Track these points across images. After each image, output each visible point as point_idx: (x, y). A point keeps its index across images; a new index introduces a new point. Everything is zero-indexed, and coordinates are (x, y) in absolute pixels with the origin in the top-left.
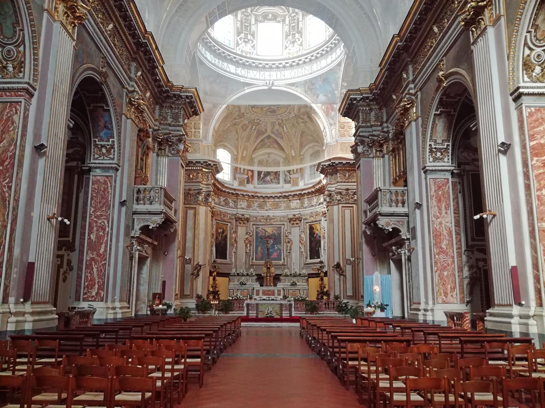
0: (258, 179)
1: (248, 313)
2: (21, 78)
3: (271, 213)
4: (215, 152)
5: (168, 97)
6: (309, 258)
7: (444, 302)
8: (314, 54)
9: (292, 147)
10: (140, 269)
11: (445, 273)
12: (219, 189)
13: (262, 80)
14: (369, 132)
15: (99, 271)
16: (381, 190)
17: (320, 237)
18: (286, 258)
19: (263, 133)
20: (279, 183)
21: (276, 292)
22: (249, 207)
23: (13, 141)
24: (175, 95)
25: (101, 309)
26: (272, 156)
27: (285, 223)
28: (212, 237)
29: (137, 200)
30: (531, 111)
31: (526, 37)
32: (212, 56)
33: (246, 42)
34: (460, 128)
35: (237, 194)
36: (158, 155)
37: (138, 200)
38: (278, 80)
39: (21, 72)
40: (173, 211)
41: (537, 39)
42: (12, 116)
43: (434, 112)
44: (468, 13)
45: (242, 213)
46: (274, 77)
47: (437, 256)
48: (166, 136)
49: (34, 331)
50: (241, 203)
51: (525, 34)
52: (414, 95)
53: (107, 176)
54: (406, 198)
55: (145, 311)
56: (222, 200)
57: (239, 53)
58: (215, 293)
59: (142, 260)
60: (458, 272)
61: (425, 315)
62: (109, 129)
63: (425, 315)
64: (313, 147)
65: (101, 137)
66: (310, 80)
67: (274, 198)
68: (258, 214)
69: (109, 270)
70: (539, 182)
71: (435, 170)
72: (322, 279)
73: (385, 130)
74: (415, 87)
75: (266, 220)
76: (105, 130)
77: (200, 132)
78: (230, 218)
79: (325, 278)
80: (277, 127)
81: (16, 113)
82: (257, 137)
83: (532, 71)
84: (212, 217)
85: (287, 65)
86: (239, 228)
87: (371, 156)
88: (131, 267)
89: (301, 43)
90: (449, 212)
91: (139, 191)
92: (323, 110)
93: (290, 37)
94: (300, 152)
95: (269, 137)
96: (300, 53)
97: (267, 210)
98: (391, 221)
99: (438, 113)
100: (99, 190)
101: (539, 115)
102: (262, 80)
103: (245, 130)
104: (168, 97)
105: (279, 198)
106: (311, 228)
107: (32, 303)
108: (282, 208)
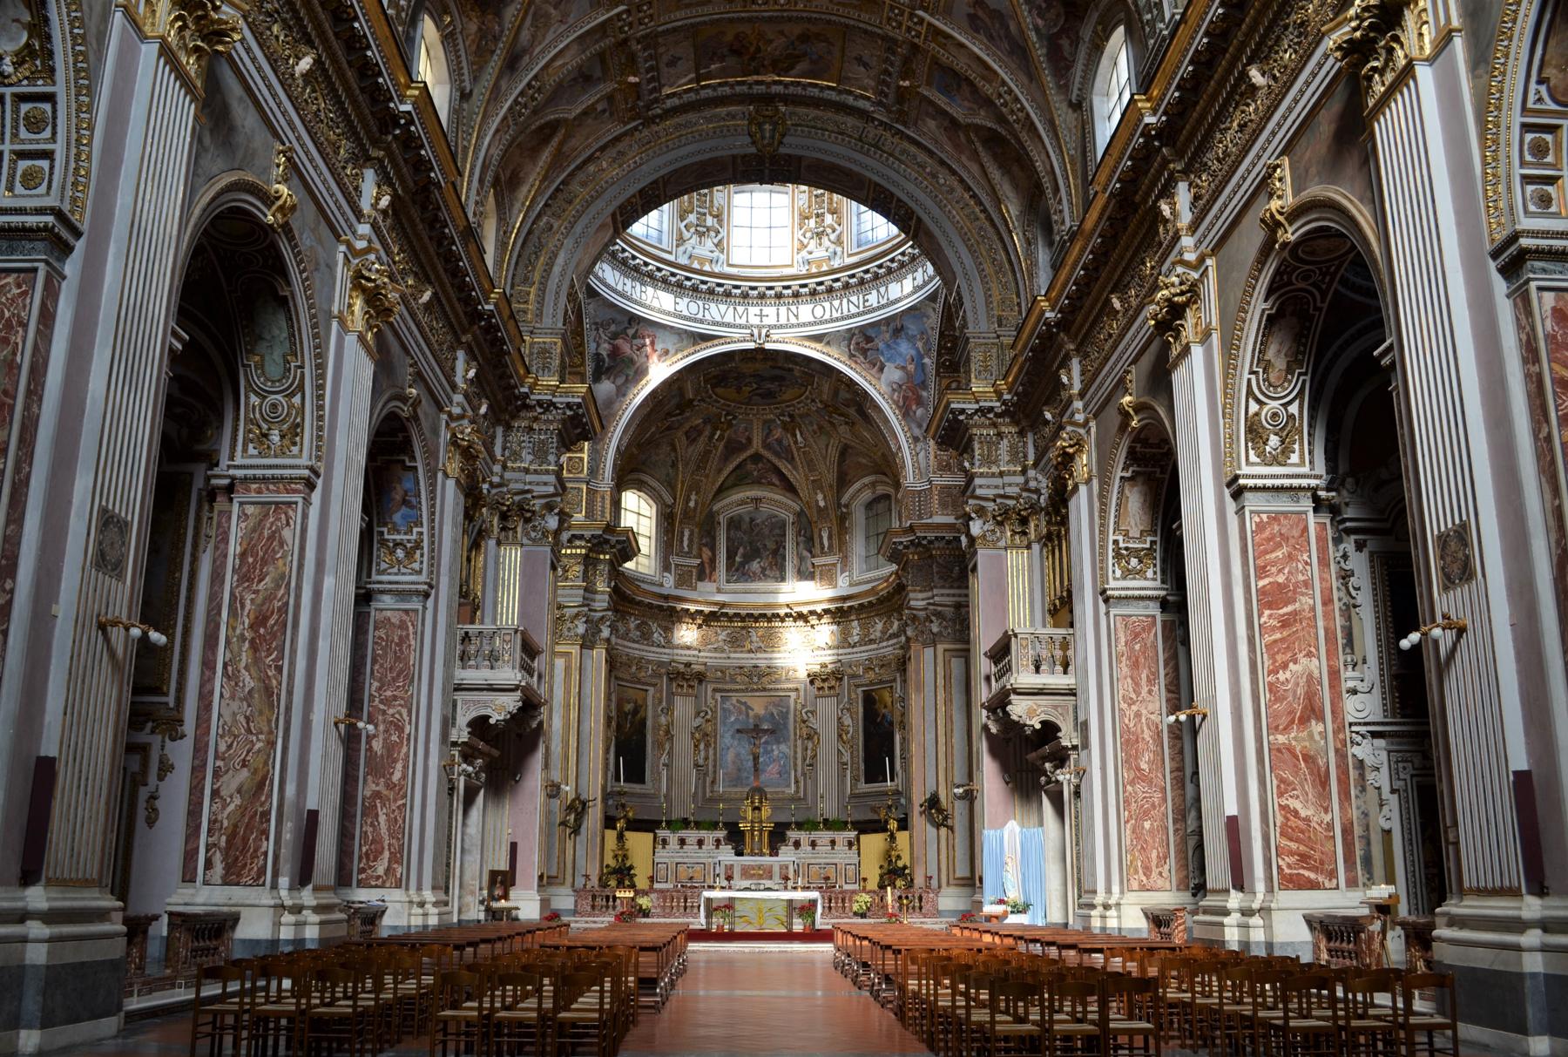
2: (294, 457)
4: (617, 504)
7: (1143, 888)
9: (817, 485)
11: (1147, 825)
13: (740, 327)
17: (891, 724)
21: (776, 870)
23: (282, 579)
24: (540, 403)
25: (398, 906)
29: (462, 659)
31: (1249, 380)
32: (617, 274)
33: (701, 235)
34: (1336, 356)
36: (499, 543)
37: (464, 657)
38: (781, 327)
39: (295, 444)
41: (1270, 385)
42: (278, 530)
43: (1119, 474)
44: (1353, 24)
45: (685, 659)
46: (771, 320)
48: (517, 498)
49: (321, 940)
51: (1246, 376)
52: (1195, 268)
53: (406, 611)
55: (476, 913)
56: (632, 626)
57: (683, 261)
58: (623, 874)
61: (1103, 917)
62: (412, 507)
63: (1103, 917)
64: (873, 484)
70: (1272, 657)
71: (1127, 598)
72: (893, 837)
73: (1033, 484)
74: (1085, 408)
75: (750, 676)
76: (404, 510)
77: (581, 459)
80: (778, 433)
81: (288, 524)
82: (726, 458)
83: (1265, 444)
85: (803, 290)
86: (678, 700)
87: (1002, 544)
88: (451, 813)
89: (839, 237)
91: (466, 638)
92: (896, 403)
94: (839, 499)
95: (757, 458)
96: (836, 263)
97: (750, 651)
99: (1128, 474)
100: (389, 641)
101: (1276, 528)
102: (740, 327)
103: (694, 440)
106: (869, 700)
107: (315, 889)
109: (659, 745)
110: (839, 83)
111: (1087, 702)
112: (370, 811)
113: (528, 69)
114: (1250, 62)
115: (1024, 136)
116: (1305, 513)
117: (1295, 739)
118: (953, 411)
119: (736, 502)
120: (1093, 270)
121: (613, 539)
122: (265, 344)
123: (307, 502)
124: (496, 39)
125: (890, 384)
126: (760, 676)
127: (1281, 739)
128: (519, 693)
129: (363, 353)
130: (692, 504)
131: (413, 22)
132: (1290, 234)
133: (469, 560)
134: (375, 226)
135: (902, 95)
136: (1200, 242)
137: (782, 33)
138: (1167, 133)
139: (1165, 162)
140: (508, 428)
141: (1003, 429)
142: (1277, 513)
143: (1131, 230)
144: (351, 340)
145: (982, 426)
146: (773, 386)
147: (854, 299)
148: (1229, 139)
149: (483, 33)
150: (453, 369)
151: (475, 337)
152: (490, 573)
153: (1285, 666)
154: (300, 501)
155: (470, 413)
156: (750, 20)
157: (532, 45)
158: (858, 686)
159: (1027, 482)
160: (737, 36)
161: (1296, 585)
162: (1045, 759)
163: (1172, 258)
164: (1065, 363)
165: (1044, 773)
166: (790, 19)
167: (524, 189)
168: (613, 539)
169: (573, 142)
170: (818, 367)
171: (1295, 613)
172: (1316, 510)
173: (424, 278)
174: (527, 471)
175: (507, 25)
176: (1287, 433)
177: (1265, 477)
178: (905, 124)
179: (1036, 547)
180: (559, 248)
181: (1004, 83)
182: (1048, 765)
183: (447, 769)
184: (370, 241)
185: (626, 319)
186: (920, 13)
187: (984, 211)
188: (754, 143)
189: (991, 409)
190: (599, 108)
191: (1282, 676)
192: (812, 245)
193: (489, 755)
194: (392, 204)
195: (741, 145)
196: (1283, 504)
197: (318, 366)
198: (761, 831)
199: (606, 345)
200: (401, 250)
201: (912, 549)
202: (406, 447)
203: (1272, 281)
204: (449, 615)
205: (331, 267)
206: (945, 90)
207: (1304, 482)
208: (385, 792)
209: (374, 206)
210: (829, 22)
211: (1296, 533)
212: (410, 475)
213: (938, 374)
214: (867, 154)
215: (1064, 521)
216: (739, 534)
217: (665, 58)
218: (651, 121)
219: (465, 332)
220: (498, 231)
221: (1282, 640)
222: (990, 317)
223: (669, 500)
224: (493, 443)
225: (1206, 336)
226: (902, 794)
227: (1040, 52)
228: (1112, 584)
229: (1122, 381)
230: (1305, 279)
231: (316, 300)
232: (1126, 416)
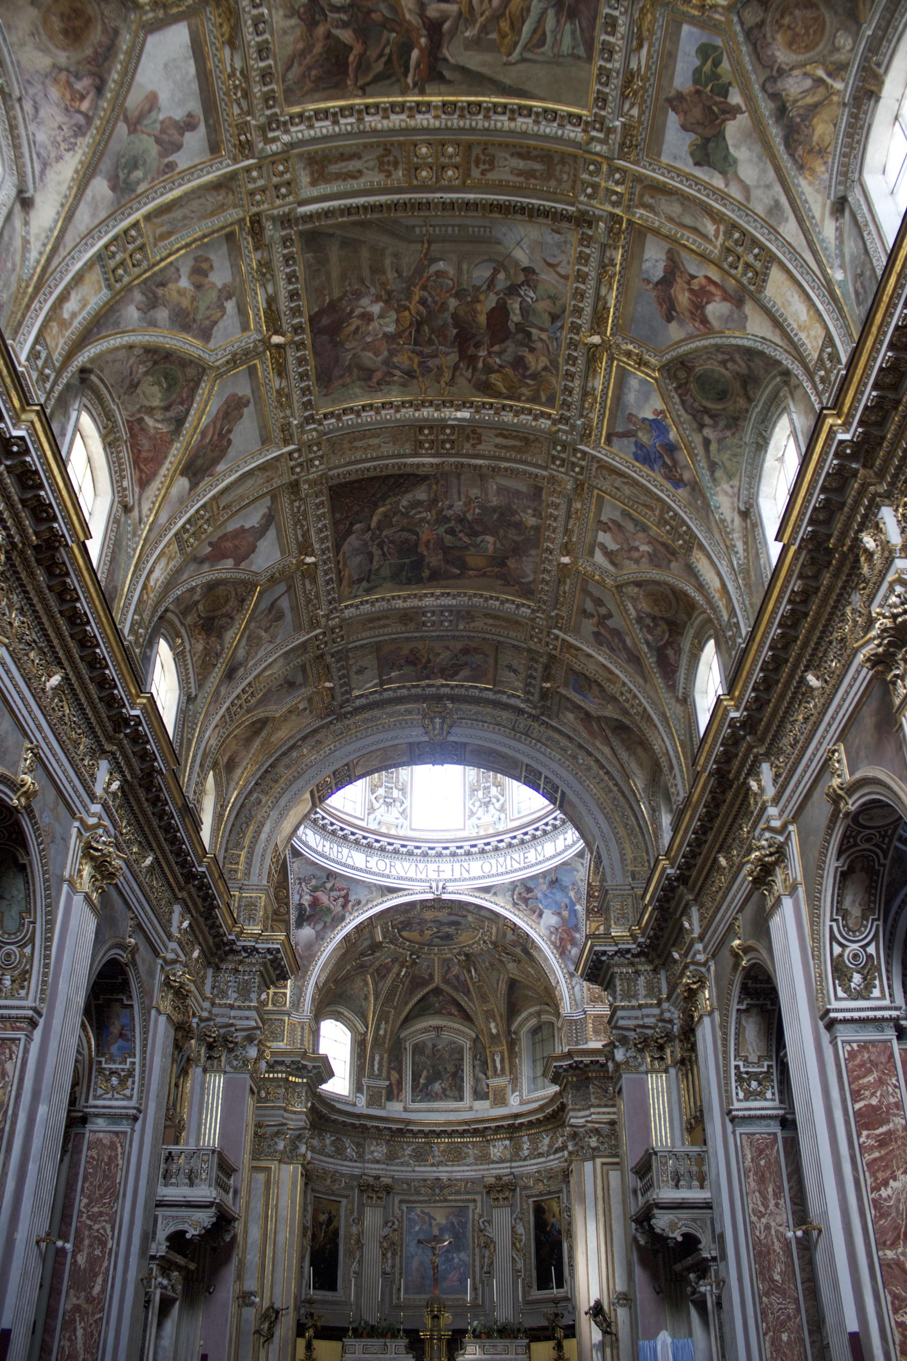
0: (414, 1089)
2: (21, 999)
3: (444, 1173)
4: (316, 1033)
5: (232, 951)
6: (535, 1286)
8: (530, 830)
10: (160, 1325)
12: (325, 1116)
15: (88, 1335)
16: (656, 1153)
17: (559, 1232)
18: (480, 1286)
19: (424, 983)
22: (391, 1157)
24: (244, 949)
26: (445, 1035)
27: (478, 1197)
28: (304, 1235)
29: (165, 1177)
33: (388, 805)
35: (364, 1126)
36: (205, 1071)
37: (166, 1175)
38: (455, 880)
39: (22, 988)
40: (231, 1195)
46: (447, 875)
47: (765, 1299)
48: (222, 1031)
51: (828, 923)
53: (117, 1133)
56: (328, 1142)
57: (373, 826)
59: (166, 1305)
60: (811, 1333)
62: (128, 1040)
64: (539, 1014)
65: (112, 1055)
66: (523, 882)
67: (450, 1134)
69: (106, 1333)
70: (873, 1174)
71: (750, 1117)
72: (559, 1347)
73: (667, 1015)
74: (705, 948)
76: (120, 1042)
77: (285, 994)
78: (349, 1187)
79: (566, 1343)
82: (411, 992)
84: (306, 1184)
86: (368, 1211)
87: (643, 1068)
88: (146, 1325)
90: (781, 1202)
91: (170, 1157)
92: (554, 944)
93: (480, 794)
95: (437, 991)
97: (433, 1165)
99: (743, 1007)
101: (866, 1055)
102: (421, 880)
104: (232, 951)
105: (462, 1134)
106: (539, 1211)
108: (471, 1160)
109: (350, 1253)
111: (722, 1215)
112: (69, 1324)
113: (243, 679)
114: (807, 668)
115: (643, 725)
116: (890, 1041)
117: (903, 1254)
120: (704, 830)
122: (5, 903)
123: (29, 1038)
124: (218, 655)
125: (548, 928)
126: (442, 1188)
127: (890, 1254)
128: (213, 1209)
129: (87, 910)
131: (151, 643)
132: (852, 805)
133: (177, 1086)
134: (105, 806)
135: (545, 695)
136: (782, 811)
137: (447, 648)
138: (749, 724)
139: (750, 748)
140: (218, 969)
141: (640, 967)
142: (865, 1042)
143: (724, 803)
144: (78, 899)
146: (451, 930)
147: (516, 856)
148: (796, 729)
149: (207, 652)
150: (170, 921)
152: (196, 1097)
153: (886, 1184)
154: (23, 1037)
155: (183, 958)
157: (246, 660)
158: (529, 1197)
159: (662, 1013)
160: (411, 651)
161: (888, 1107)
162: (689, 1269)
163: (762, 825)
164: (685, 912)
165: (689, 1283)
166: (454, 637)
167: (238, 772)
170: (487, 914)
171: (889, 1133)
172: (899, 1038)
173: (147, 846)
174: (232, 1007)
175: (227, 645)
176: (869, 970)
177: (852, 1010)
178: (549, 717)
179: (672, 1071)
181: (624, 684)
182: (692, 1276)
183: (145, 1281)
184: (100, 818)
185: (324, 875)
186: (556, 631)
187: (616, 785)
189: (628, 951)
190: (301, 706)
191: (884, 1193)
192: (480, 812)
193: (186, 1268)
194: (121, 788)
196: (870, 1035)
197: (48, 922)
200: (129, 824)
201: (571, 1072)
202: (124, 988)
203: (841, 844)
204: (155, 1138)
205: (65, 840)
206: (578, 690)
207: (886, 1014)
208: (85, 1306)
209: (106, 790)
211: (883, 1059)
213: (588, 918)
214: (519, 740)
215: (693, 1048)
216: (423, 1059)
217: (354, 668)
218: (342, 717)
221: (881, 1158)
222: (624, 871)
223: (362, 1029)
224: (203, 983)
225: (792, 890)
226: (570, 1300)
227: (650, 661)
228: (737, 1105)
229: (731, 926)
230: (868, 840)
231: (51, 868)
232: (736, 956)
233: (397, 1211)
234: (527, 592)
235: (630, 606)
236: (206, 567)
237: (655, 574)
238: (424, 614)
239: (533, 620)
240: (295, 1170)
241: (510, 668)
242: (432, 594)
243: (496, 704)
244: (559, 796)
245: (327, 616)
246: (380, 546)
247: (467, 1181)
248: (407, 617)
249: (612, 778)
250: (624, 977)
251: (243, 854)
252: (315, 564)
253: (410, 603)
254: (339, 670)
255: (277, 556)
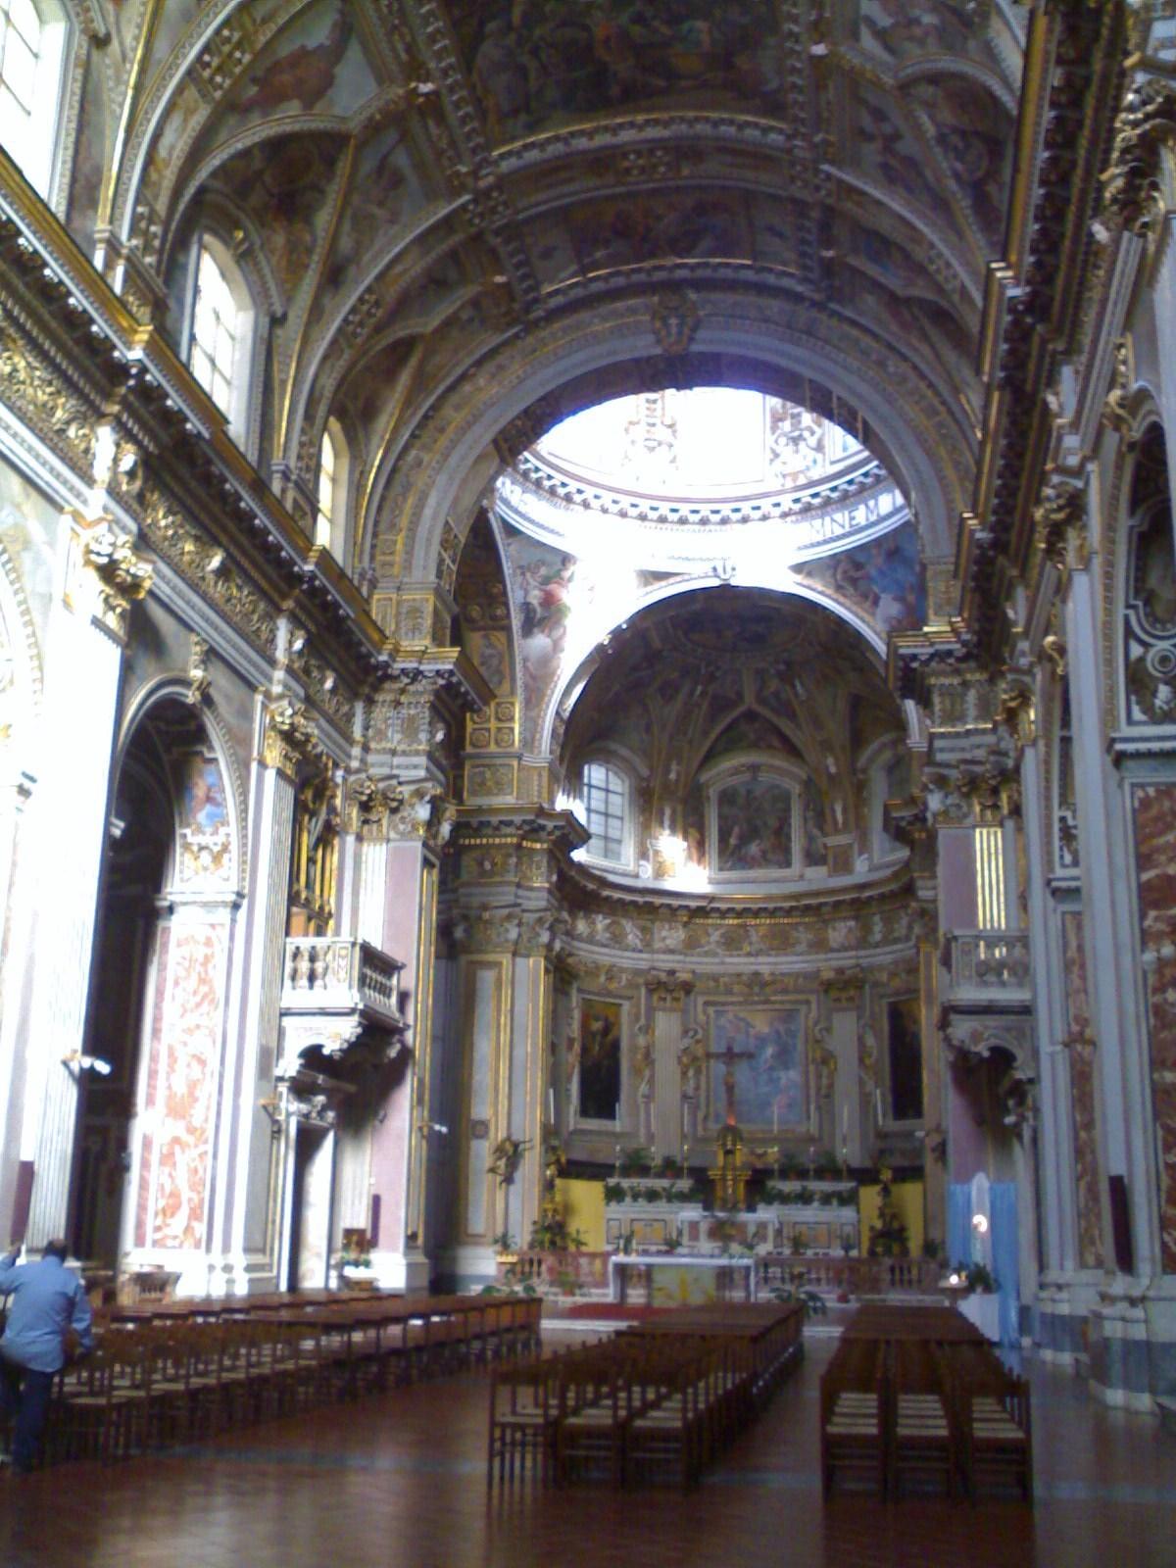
1: (623, 1295)
9: (827, 746)
14: (963, 750)
19: (730, 704)
20: (788, 864)
22: (691, 945)
26: (764, 777)
30: (1147, 796)
36: (360, 838)
48: (381, 785)
50: (664, 933)
54: (289, 965)
55: (316, 1277)
59: (307, 1144)
66: (849, 554)
68: (720, 969)
73: (1003, 745)
76: (208, 808)
77: (512, 730)
78: (631, 985)
80: (774, 685)
82: (712, 718)
87: (969, 821)
93: (786, 426)
95: (751, 716)
97: (749, 954)
98: (986, 1028)
101: (1167, 804)
105: (789, 912)
110: (755, 259)
112: (168, 1159)
118: (902, 657)
119: (726, 771)
121: (550, 825)
124: (309, 251)
126: (764, 985)
130: (673, 776)
135: (828, 268)
141: (969, 677)
145: (943, 674)
147: (838, 516)
149: (292, 247)
151: (298, 602)
156: (630, 195)
158: (882, 997)
166: (678, 189)
168: (550, 825)
169: (437, 359)
173: (208, 539)
174: (393, 753)
175: (320, 234)
180: (430, 486)
183: (269, 1111)
185: (558, 560)
186: (825, 167)
188: (659, 341)
189: (949, 653)
190: (464, 316)
195: (644, 346)
198: (734, 1180)
199: (536, 592)
206: (875, 258)
210: (724, 188)
212: (212, 767)
218: (532, 326)
219: (284, 596)
220: (351, 472)
225: (1086, 563)
227: (963, 204)
228: (1059, 872)
233: (702, 1017)
234: (774, 106)
235: (925, 119)
236: (255, 118)
237: (947, 63)
238: (625, 156)
239: (789, 151)
240: (536, 964)
241: (771, 229)
242: (632, 125)
243: (761, 289)
244: (860, 425)
245: (475, 174)
246: (535, 52)
247: (797, 975)
248: (601, 162)
249: (938, 394)
250: (947, 692)
251: (400, 539)
252: (436, 93)
253: (601, 140)
254: (511, 255)
255: (371, 87)
